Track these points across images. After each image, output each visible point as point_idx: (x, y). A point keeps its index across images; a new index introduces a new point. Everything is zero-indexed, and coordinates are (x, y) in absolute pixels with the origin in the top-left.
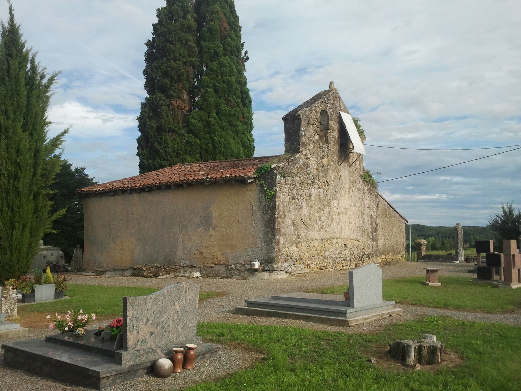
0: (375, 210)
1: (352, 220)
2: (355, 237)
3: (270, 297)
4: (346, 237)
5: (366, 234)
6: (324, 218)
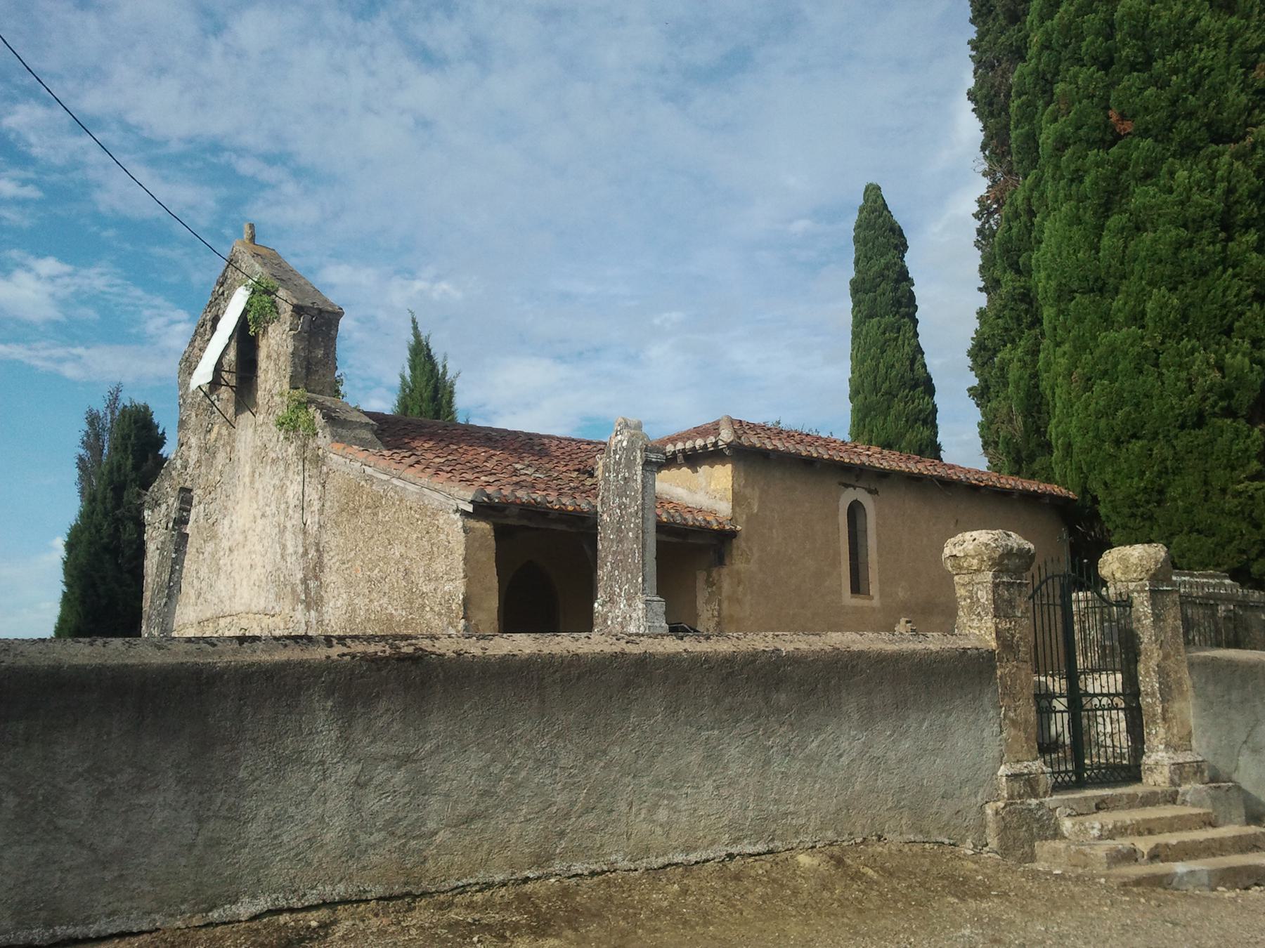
0: (316, 506)
1: (258, 560)
5: (289, 588)
6: (204, 572)
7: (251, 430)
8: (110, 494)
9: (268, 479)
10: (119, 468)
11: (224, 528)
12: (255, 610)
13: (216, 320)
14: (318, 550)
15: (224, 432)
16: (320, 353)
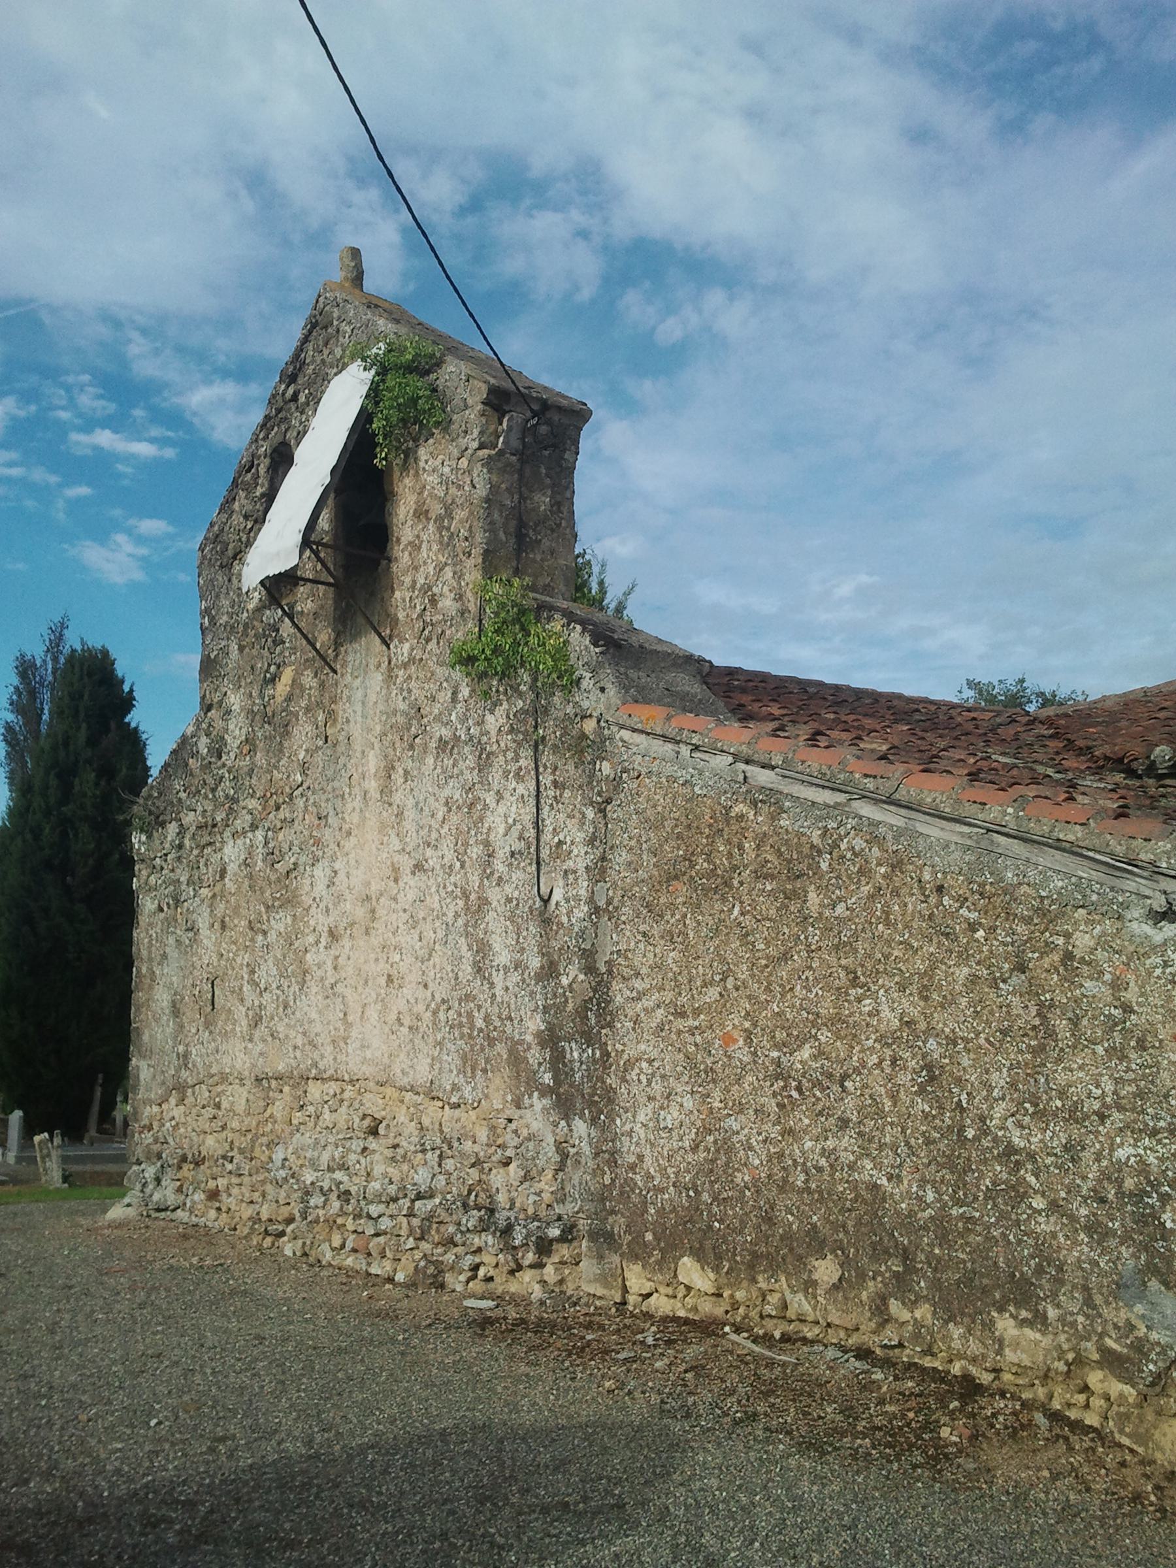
0: (580, 858)
1: (406, 965)
2: (422, 1073)
3: (534, 355)
4: (368, 1070)
5: (501, 1049)
6: (267, 972)
7: (378, 678)
8: (53, 782)
9: (429, 788)
10: (66, 744)
11: (314, 883)
12: (405, 1081)
13: (282, 459)
14: (590, 969)
15: (308, 679)
16: (543, 501)
